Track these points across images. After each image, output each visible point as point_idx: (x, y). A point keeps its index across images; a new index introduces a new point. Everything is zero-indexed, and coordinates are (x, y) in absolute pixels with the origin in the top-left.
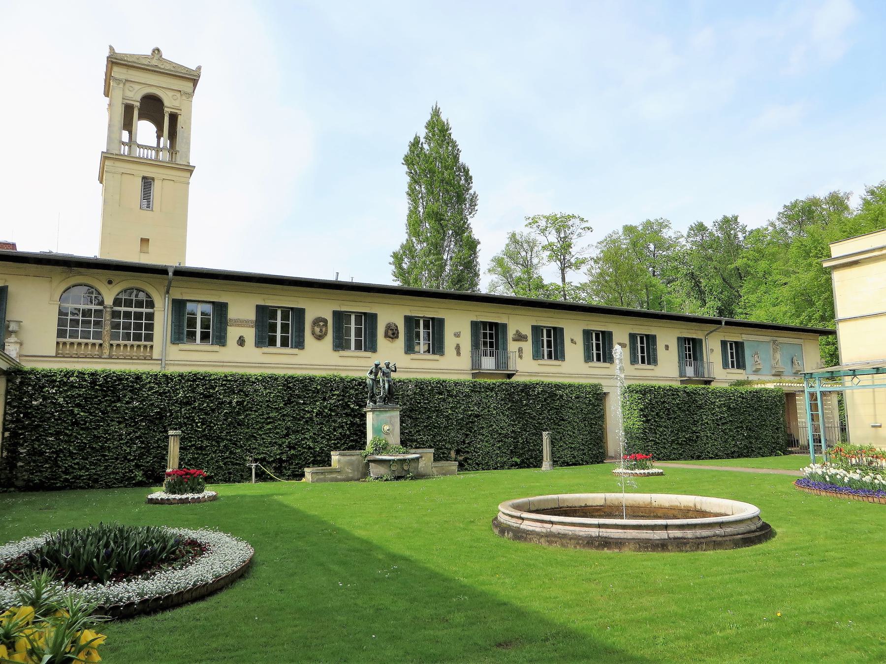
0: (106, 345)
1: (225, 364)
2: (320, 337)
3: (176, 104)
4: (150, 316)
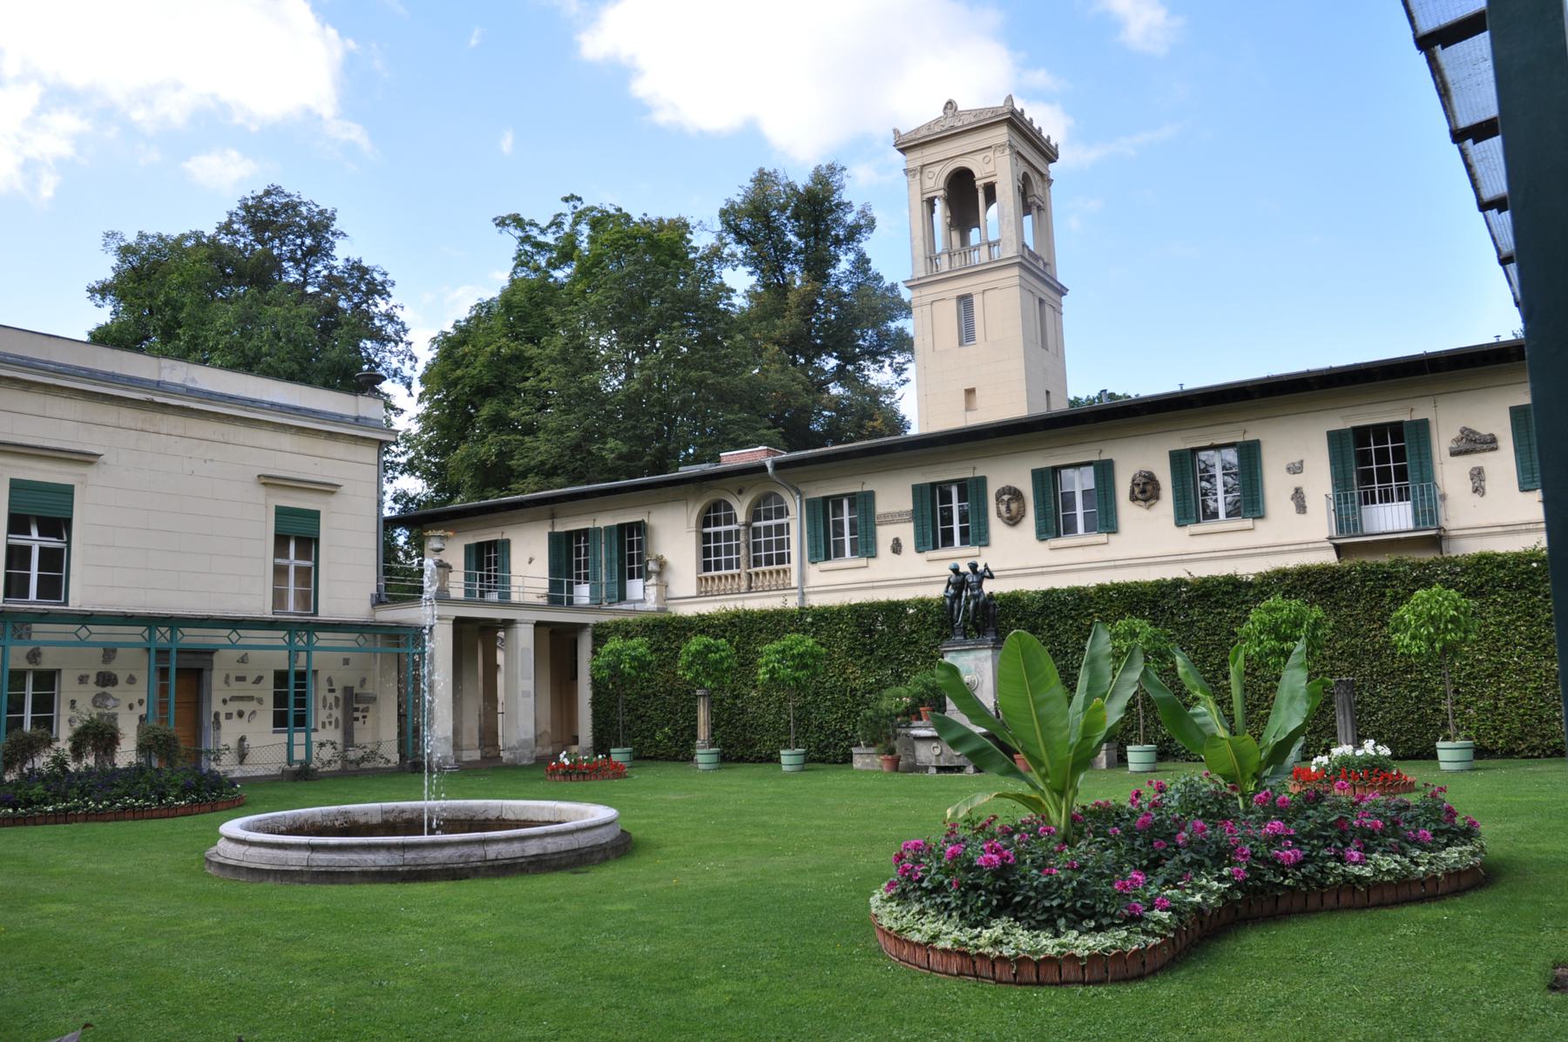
0: (743, 575)
1: (875, 584)
2: (1013, 520)
3: (989, 169)
4: (781, 529)
